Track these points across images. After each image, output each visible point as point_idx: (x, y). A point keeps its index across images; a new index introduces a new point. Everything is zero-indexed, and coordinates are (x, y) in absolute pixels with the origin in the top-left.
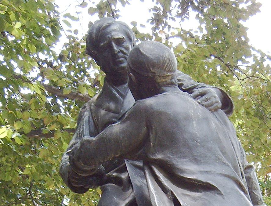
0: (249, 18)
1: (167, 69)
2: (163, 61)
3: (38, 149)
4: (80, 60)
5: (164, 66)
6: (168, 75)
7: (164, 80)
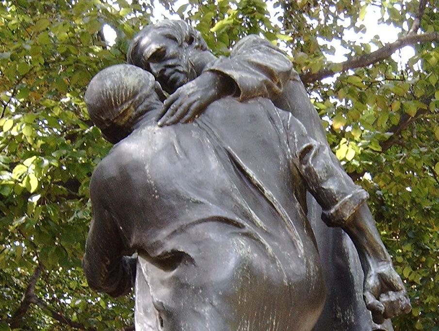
0: (115, 41)
1: (117, 103)
2: (106, 98)
3: (348, 217)
4: (381, 110)
5: (112, 102)
6: (124, 109)
7: (126, 118)
